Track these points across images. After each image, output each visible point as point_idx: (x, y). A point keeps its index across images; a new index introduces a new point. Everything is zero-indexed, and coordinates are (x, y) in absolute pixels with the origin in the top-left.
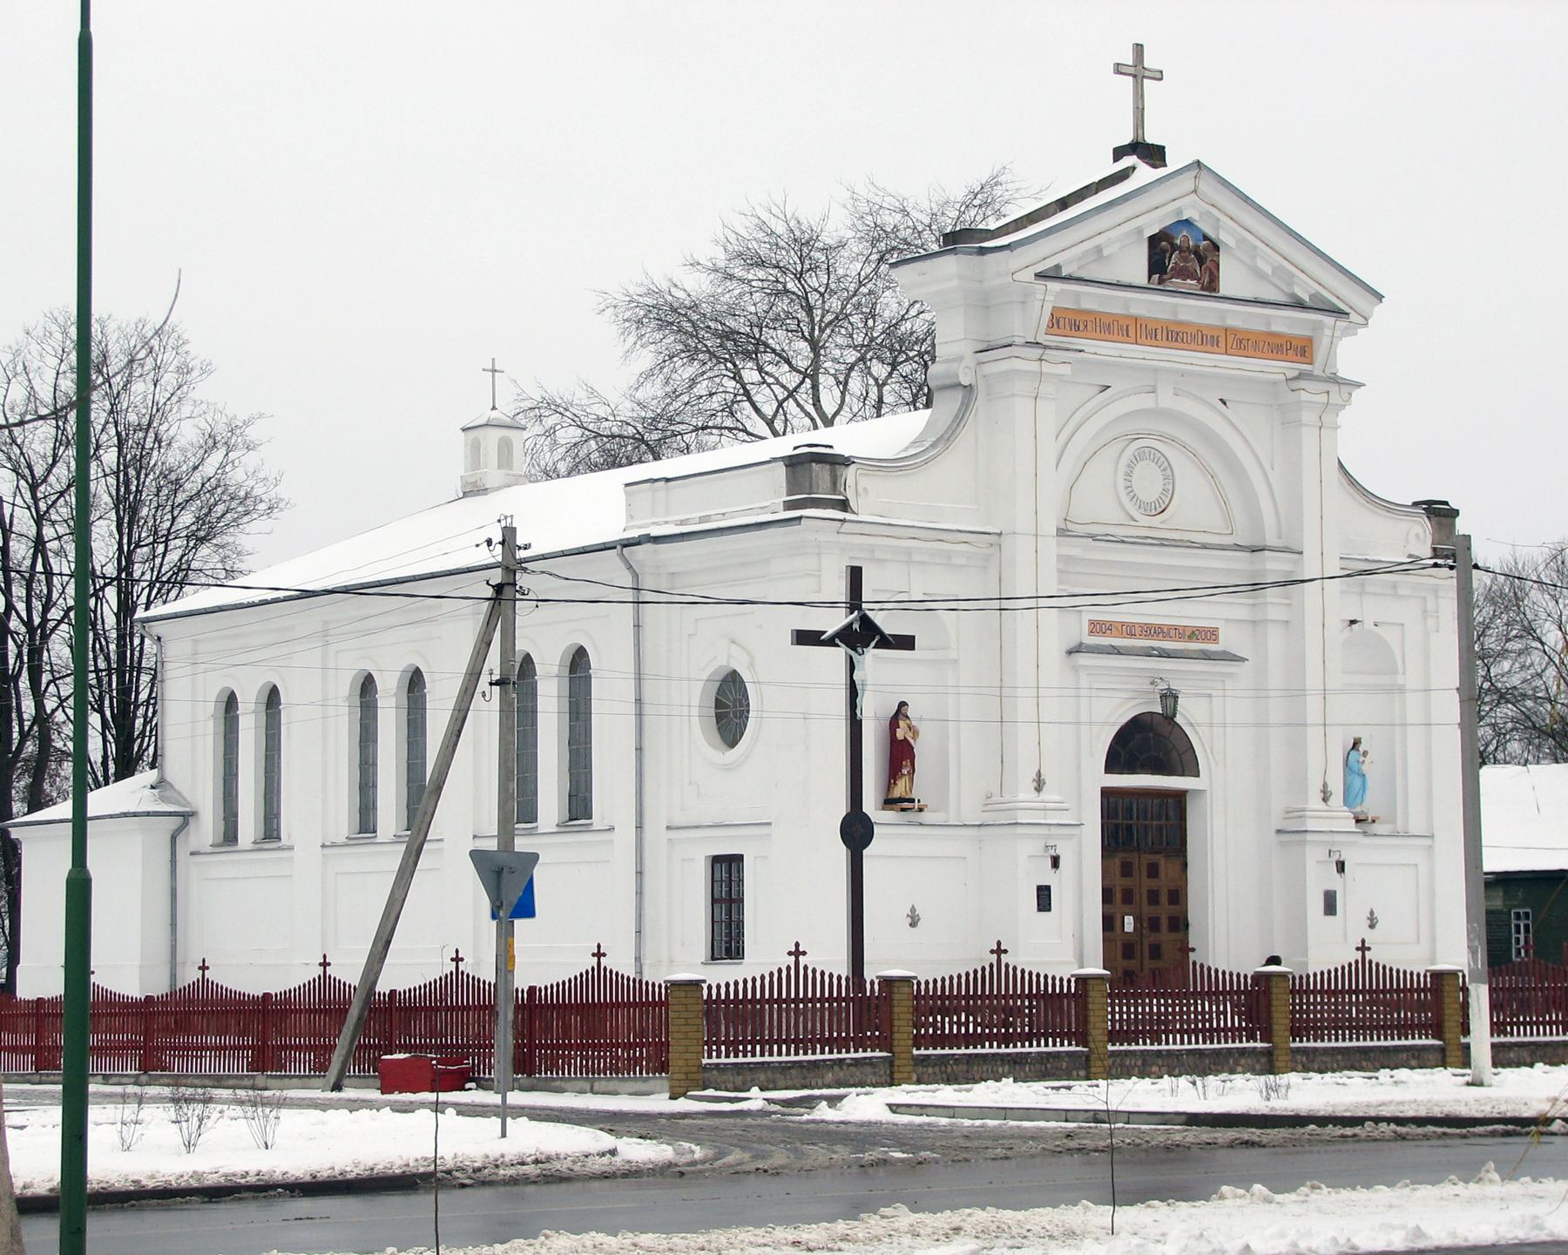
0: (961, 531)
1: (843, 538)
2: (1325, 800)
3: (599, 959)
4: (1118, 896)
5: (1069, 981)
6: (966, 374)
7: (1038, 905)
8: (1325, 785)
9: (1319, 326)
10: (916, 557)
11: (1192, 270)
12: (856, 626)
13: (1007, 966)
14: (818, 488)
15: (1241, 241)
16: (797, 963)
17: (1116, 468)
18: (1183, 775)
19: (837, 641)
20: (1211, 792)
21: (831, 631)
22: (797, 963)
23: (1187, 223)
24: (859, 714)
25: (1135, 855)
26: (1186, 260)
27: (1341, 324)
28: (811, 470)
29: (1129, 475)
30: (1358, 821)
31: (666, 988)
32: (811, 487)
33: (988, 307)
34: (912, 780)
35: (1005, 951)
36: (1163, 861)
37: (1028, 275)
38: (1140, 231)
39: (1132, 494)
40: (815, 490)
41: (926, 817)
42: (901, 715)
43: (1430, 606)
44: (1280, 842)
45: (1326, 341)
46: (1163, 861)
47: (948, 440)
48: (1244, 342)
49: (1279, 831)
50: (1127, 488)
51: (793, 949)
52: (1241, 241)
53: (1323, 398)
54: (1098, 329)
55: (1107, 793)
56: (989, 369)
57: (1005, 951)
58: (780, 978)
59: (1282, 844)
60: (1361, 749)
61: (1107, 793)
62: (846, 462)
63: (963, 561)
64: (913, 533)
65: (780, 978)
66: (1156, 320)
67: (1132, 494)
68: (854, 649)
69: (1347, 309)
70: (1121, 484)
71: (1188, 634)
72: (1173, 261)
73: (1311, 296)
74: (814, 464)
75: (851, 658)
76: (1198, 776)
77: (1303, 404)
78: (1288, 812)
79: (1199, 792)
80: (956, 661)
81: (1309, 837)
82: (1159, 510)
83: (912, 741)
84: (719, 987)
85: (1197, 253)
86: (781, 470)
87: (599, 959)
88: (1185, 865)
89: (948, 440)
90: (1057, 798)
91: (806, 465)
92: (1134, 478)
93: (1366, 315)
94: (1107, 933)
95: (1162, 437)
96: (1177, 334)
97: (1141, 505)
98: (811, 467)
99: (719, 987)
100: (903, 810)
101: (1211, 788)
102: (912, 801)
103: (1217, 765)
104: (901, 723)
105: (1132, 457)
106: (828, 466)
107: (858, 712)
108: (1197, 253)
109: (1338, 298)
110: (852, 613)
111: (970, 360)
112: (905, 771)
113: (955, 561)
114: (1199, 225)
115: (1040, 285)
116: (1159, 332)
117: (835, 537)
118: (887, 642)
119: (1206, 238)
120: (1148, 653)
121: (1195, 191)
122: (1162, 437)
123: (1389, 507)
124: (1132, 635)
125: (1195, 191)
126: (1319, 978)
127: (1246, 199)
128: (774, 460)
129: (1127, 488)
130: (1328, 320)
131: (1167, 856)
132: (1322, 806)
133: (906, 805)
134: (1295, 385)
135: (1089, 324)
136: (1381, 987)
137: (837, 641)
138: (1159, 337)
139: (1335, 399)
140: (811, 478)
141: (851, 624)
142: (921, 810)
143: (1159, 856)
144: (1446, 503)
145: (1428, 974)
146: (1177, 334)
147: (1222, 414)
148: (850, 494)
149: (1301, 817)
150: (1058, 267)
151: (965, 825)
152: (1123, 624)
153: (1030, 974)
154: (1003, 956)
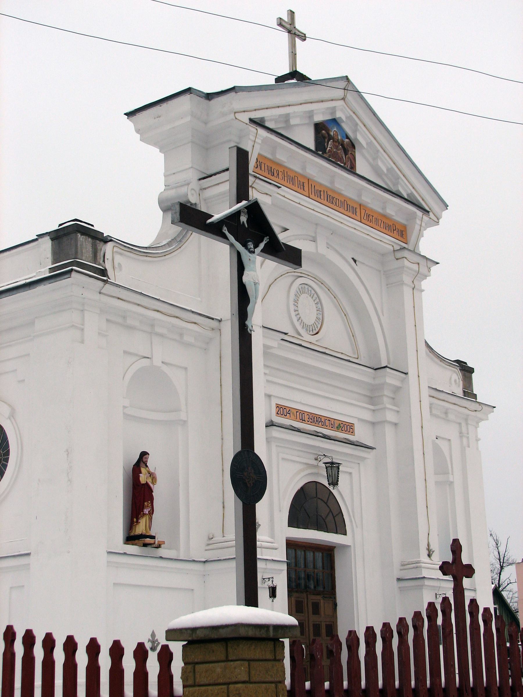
0: (193, 312)
1: (104, 298)
2: (429, 556)
6: (192, 194)
9: (413, 217)
10: (158, 330)
11: (340, 156)
14: (82, 255)
15: (370, 144)
16: (459, 591)
17: (289, 291)
18: (337, 533)
19: (225, 230)
20: (355, 548)
21: (217, 217)
22: (459, 591)
23: (335, 121)
25: (305, 595)
26: (337, 147)
27: (425, 218)
28: (76, 240)
29: (296, 301)
32: (76, 253)
33: (207, 149)
34: (151, 519)
36: (322, 601)
37: (245, 118)
38: (310, 114)
39: (298, 316)
40: (79, 256)
41: (162, 552)
42: (142, 463)
43: (464, 429)
44: (399, 588)
45: (417, 227)
46: (322, 601)
47: (180, 241)
48: (371, 217)
49: (398, 579)
52: (370, 144)
53: (415, 267)
54: (286, 178)
56: (208, 193)
59: (401, 589)
62: (106, 240)
63: (191, 340)
64: (157, 304)
66: (321, 185)
67: (298, 316)
68: (245, 245)
70: (292, 308)
71: (336, 425)
72: (329, 146)
73: (408, 195)
74: (79, 235)
75: (239, 255)
76: (346, 535)
77: (405, 269)
78: (403, 565)
79: (345, 547)
80: (185, 422)
81: (427, 582)
82: (315, 332)
83: (151, 485)
85: (342, 145)
86: (47, 244)
88: (335, 605)
89: (180, 241)
90: (269, 539)
91: (73, 236)
92: (299, 305)
93: (438, 216)
95: (315, 278)
97: (305, 326)
98: (77, 236)
100: (145, 545)
101: (354, 544)
102: (153, 537)
103: (357, 527)
104: (143, 470)
105: (298, 290)
106: (90, 239)
108: (342, 145)
109: (423, 200)
110: (238, 201)
111: (195, 185)
112: (146, 511)
113: (187, 338)
114: (344, 125)
115: (252, 129)
116: (322, 193)
117: (97, 296)
119: (347, 137)
120: (316, 435)
121: (343, 99)
122: (315, 278)
123: (442, 359)
124: (303, 420)
125: (343, 99)
127: (375, 114)
128: (40, 236)
130: (419, 213)
131: (324, 597)
133: (148, 540)
134: (399, 255)
135: (280, 174)
137: (225, 230)
138: (322, 197)
139: (423, 270)
140: (76, 246)
142: (159, 546)
143: (318, 597)
144: (466, 363)
147: (354, 270)
148: (108, 266)
149: (417, 567)
151: (194, 561)
152: (298, 411)
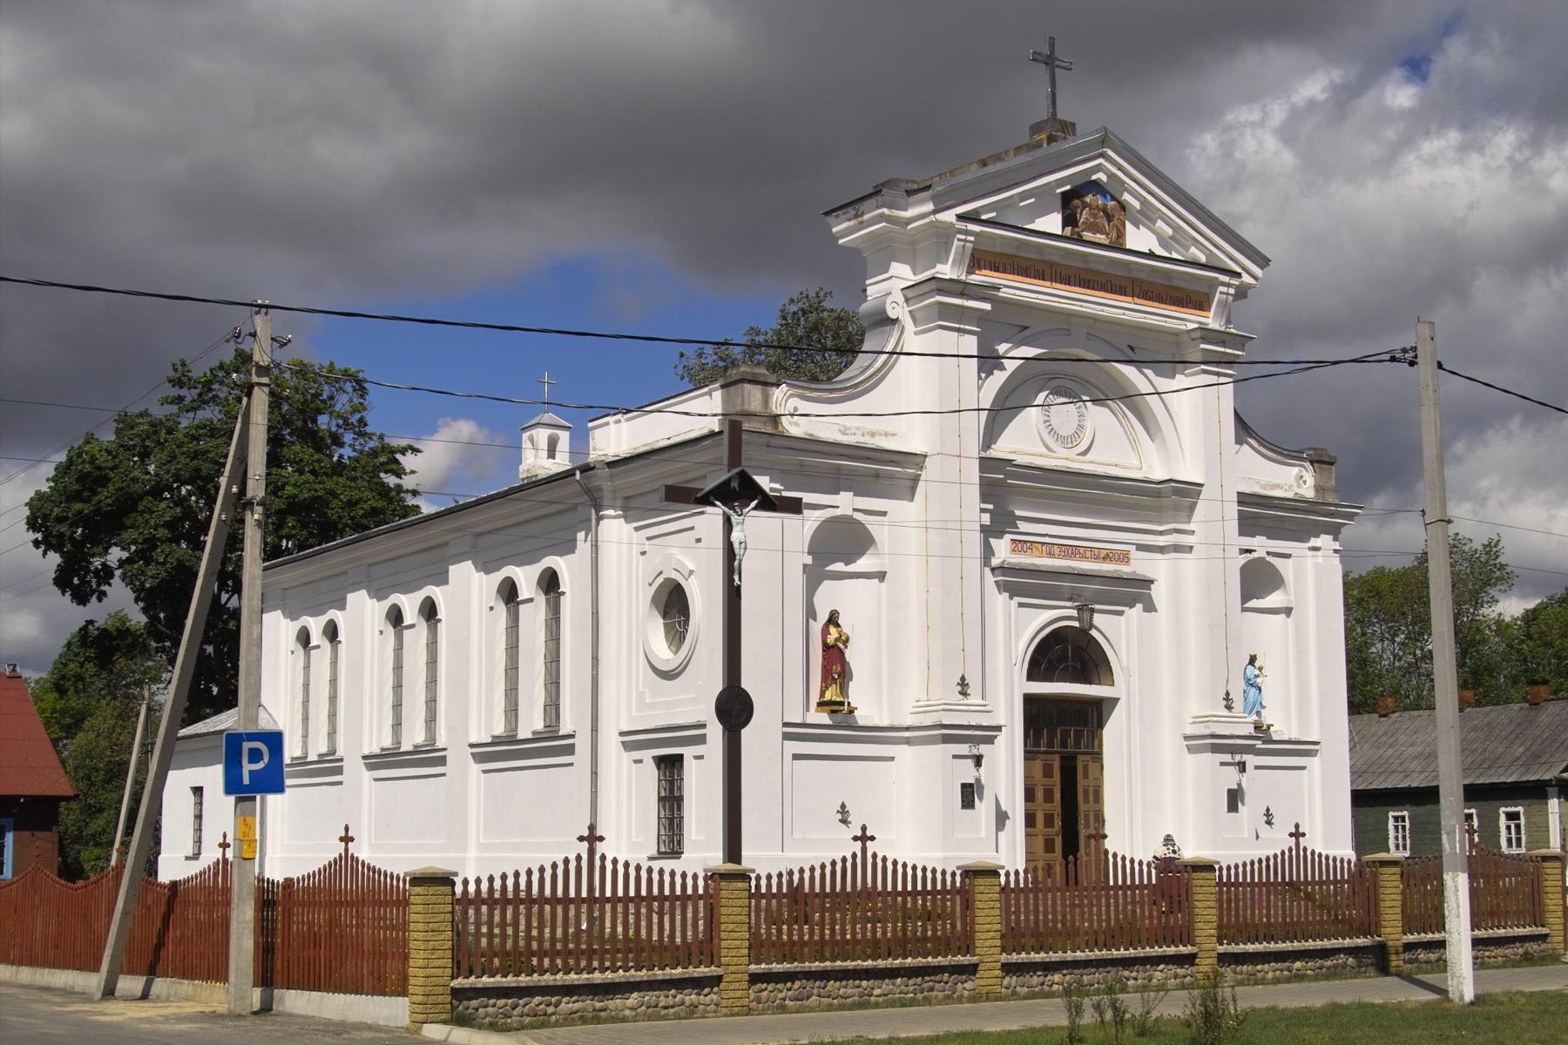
3: (347, 844)
4: (1040, 795)
5: (953, 874)
7: (963, 801)
8: (1228, 694)
12: (735, 484)
13: (875, 856)
16: (591, 852)
19: (712, 498)
22: (591, 852)
24: (737, 581)
26: (1095, 216)
28: (743, 390)
30: (1256, 728)
31: (706, 878)
35: (872, 838)
50: (1045, 422)
51: (586, 833)
55: (1029, 700)
57: (872, 838)
58: (1268, 866)
60: (1257, 664)
61: (1029, 700)
65: (1268, 866)
69: (1239, 270)
72: (1083, 216)
79: (1115, 701)
84: (769, 877)
85: (1105, 211)
87: (347, 844)
94: (1030, 829)
96: (1089, 281)
99: (769, 877)
107: (736, 577)
118: (769, 504)
126: (1241, 870)
129: (1045, 422)
132: (1226, 712)
136: (1249, 880)
137: (712, 498)
140: (743, 396)
141: (728, 481)
145: (408, 878)
146: (1089, 281)
150: (977, 211)
153: (905, 866)
154: (869, 843)
